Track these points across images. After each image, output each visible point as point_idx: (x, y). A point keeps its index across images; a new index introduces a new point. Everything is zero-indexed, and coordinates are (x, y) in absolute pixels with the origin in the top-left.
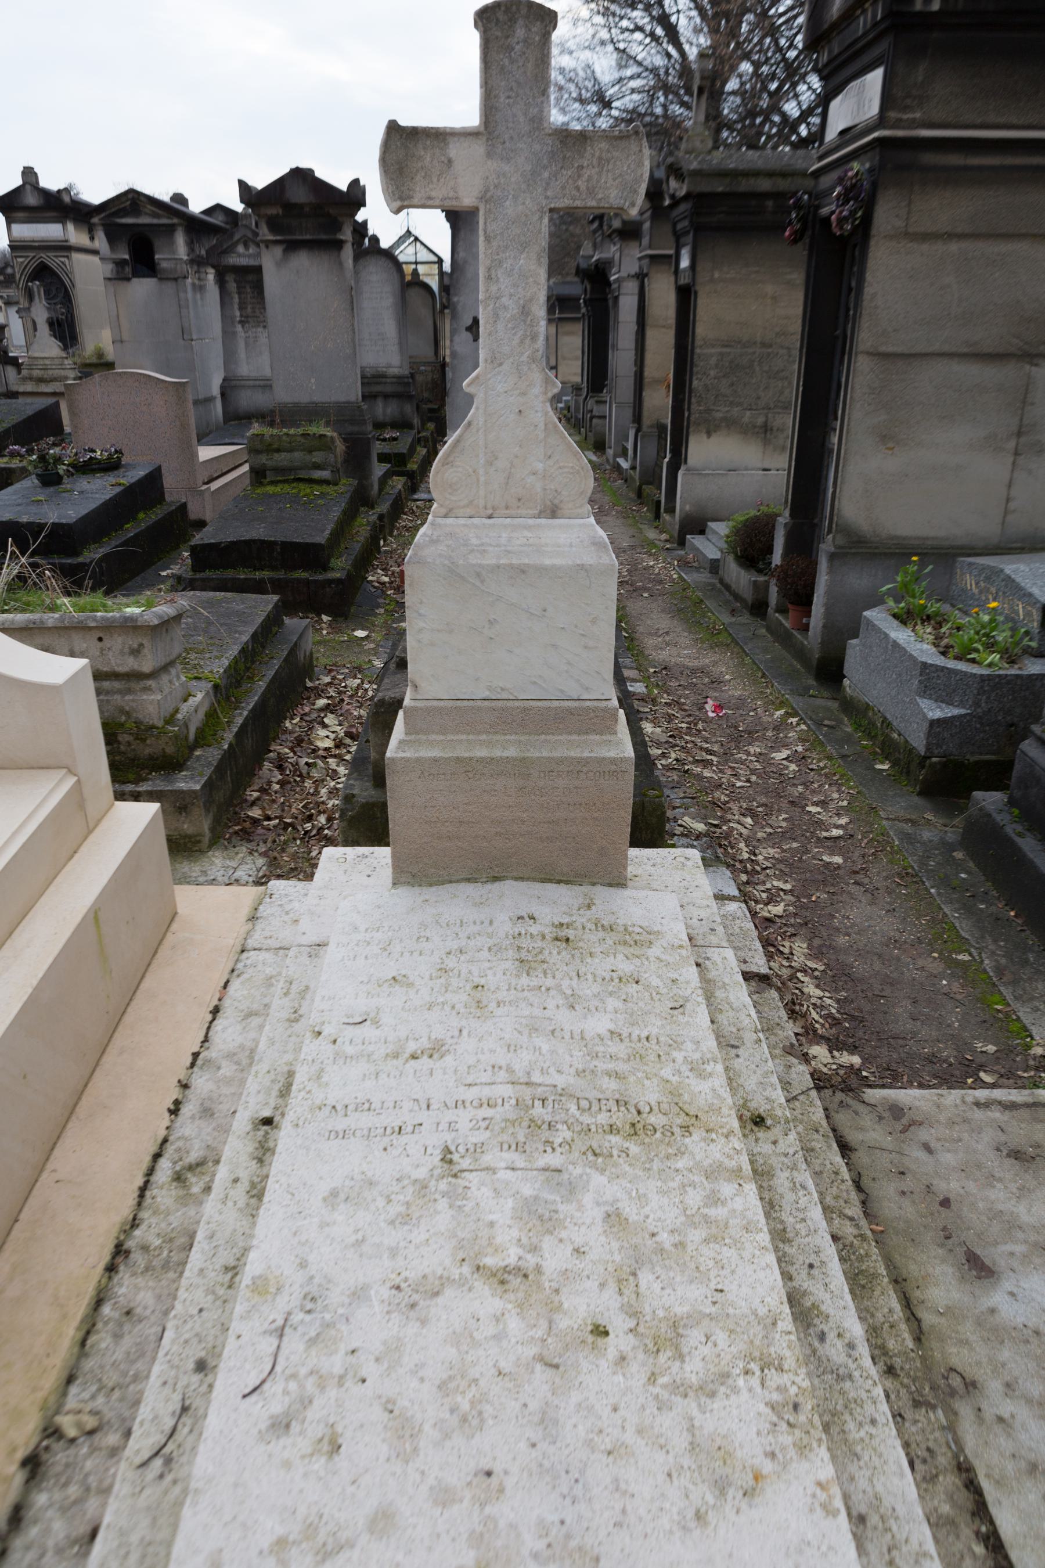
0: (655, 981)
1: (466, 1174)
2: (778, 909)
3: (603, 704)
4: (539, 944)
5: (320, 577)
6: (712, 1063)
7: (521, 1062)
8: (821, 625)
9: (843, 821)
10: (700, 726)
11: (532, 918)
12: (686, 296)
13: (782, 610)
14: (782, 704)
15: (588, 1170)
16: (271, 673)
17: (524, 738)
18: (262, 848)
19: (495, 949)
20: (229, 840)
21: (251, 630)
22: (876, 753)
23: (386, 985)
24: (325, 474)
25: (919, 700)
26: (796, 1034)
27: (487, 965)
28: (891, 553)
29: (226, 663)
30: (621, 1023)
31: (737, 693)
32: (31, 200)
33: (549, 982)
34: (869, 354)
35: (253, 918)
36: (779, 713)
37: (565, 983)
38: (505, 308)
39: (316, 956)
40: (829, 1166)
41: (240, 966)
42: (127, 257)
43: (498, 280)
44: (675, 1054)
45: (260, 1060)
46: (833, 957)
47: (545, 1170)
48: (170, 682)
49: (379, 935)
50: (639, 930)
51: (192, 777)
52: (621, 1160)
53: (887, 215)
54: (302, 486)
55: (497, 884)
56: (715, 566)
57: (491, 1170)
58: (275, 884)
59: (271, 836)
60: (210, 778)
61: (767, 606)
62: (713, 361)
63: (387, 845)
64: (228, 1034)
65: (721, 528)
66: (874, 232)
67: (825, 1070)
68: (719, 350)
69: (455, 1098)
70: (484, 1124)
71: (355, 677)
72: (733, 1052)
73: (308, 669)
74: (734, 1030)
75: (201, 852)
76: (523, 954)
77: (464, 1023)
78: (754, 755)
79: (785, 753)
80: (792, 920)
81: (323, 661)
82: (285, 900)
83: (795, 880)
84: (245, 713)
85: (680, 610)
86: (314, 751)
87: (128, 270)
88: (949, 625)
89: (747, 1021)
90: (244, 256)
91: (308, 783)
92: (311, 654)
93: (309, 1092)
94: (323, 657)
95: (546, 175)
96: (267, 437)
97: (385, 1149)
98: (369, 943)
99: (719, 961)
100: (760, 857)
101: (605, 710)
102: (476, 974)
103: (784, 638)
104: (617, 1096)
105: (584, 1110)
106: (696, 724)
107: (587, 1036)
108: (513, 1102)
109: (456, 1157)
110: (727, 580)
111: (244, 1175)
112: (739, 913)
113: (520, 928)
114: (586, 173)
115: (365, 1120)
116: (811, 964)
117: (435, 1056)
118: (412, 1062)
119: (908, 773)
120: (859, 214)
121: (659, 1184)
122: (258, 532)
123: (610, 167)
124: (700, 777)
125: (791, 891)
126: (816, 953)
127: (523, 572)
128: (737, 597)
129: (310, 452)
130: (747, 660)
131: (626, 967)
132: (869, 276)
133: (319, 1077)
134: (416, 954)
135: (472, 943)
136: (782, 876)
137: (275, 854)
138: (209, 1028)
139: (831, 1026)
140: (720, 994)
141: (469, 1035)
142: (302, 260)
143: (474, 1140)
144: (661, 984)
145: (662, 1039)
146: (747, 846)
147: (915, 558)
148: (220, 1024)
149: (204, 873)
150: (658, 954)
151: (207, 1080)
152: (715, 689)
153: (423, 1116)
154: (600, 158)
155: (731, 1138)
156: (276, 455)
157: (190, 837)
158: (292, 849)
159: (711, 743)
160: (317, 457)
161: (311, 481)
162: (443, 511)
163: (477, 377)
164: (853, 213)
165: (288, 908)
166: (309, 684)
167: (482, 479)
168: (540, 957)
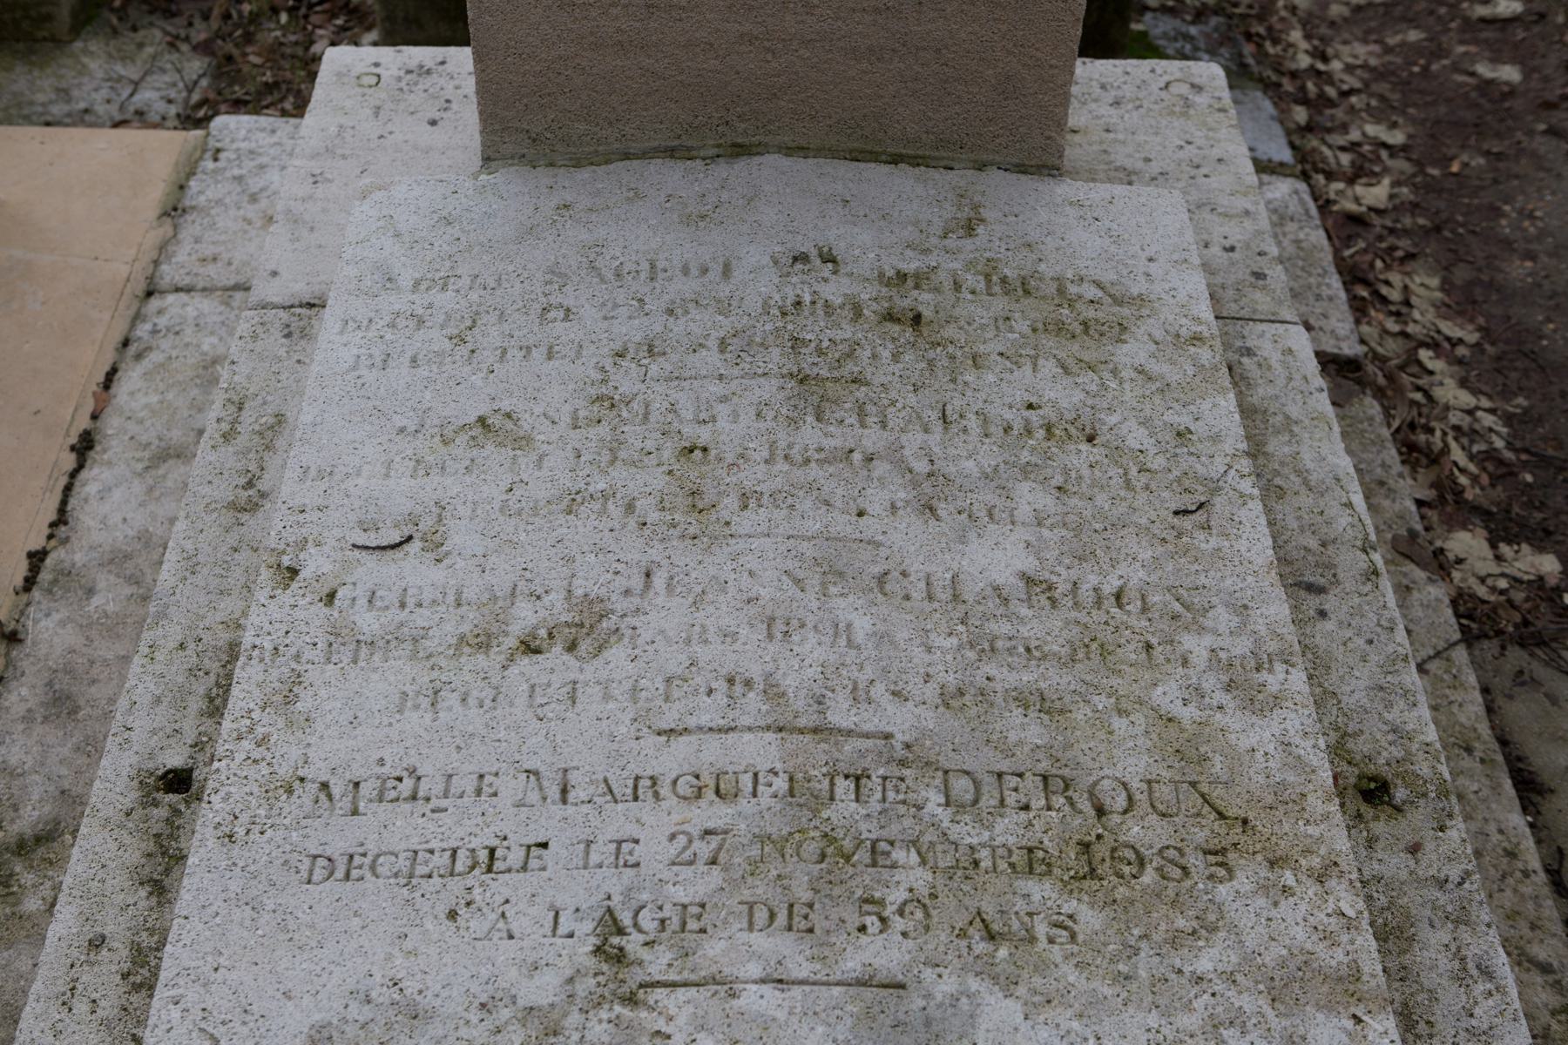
0: (1136, 437)
1: (660, 993)
2: (1376, 194)
4: (847, 332)
6: (1279, 667)
7: (801, 665)
11: (829, 259)
15: (974, 984)
18: (200, 33)
23: (462, 439)
26: (1420, 503)
27: (717, 388)
30: (1051, 555)
33: (873, 438)
35: (174, 211)
37: (913, 440)
39: (304, 334)
40: (1495, 837)
41: (143, 330)
44: (1189, 642)
45: (162, 615)
47: (861, 983)
49: (445, 300)
52: (1056, 953)
55: (741, 165)
57: (723, 984)
58: (226, 124)
63: (460, 38)
64: (112, 503)
67: (1482, 591)
69: (634, 769)
70: (704, 849)
72: (1313, 602)
74: (1313, 543)
75: (56, 41)
76: (808, 357)
77: (655, 553)
83: (1413, 121)
89: (1344, 520)
93: (262, 742)
97: (453, 915)
98: (421, 322)
99: (1275, 359)
100: (1336, 65)
104: (1044, 766)
105: (962, 807)
107: (969, 592)
108: (781, 784)
109: (632, 944)
111: (116, 927)
112: (1294, 207)
113: (798, 286)
115: (401, 829)
116: (1450, 329)
117: (584, 647)
118: (525, 662)
121: (1153, 1020)
125: (1404, 148)
126: (1460, 302)
133: (290, 699)
135: (678, 327)
137: (229, 48)
138: (68, 489)
139: (1495, 480)
140: (1277, 446)
141: (670, 587)
143: (681, 894)
144: (1148, 444)
145: (1155, 599)
148: (94, 479)
149: (64, 93)
150: (1142, 358)
151: (62, 624)
153: (548, 821)
155: (1332, 883)
158: (271, 33)
165: (255, 184)
168: (850, 368)
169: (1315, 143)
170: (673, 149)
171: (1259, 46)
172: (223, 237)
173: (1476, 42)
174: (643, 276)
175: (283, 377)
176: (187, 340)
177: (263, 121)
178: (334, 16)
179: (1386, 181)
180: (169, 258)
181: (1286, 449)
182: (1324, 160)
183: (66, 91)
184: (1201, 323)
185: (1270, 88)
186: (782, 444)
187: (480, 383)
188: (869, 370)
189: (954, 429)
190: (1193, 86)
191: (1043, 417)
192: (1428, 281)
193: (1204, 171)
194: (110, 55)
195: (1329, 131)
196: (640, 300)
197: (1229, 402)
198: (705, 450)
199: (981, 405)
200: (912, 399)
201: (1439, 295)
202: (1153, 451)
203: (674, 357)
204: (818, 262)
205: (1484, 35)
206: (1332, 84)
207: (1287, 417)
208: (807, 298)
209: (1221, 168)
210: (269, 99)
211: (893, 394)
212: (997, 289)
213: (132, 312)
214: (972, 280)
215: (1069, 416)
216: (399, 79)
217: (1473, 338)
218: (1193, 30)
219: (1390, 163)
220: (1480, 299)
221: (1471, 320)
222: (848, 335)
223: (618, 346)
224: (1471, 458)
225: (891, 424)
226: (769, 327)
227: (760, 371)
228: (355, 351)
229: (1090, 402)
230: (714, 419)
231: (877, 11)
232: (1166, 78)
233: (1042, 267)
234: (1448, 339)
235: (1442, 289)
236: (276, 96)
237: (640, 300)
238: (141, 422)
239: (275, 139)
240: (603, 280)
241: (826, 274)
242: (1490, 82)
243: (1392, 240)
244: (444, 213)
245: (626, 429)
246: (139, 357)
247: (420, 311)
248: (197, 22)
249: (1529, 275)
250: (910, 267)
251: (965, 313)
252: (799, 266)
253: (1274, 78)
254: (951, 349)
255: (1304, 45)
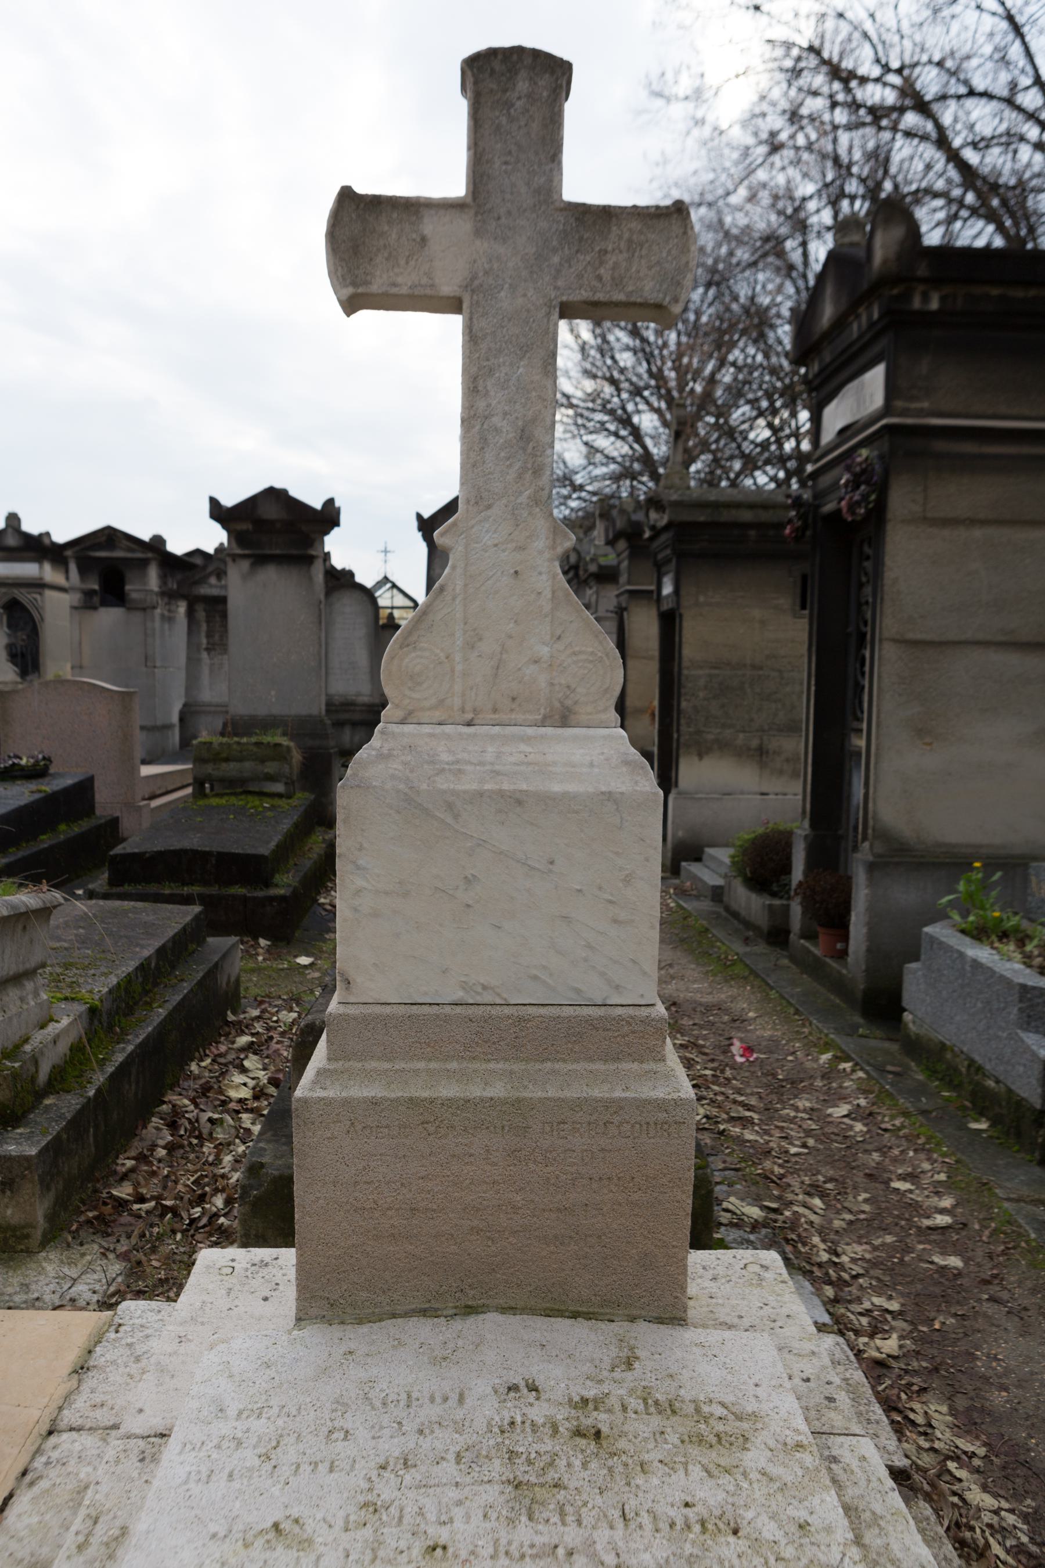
0: (770, 1530)
2: (890, 1345)
3: (644, 1012)
4: (548, 1445)
5: (260, 894)
8: (864, 948)
9: (947, 1202)
10: (728, 1073)
11: (533, 1388)
12: (670, 623)
13: (809, 935)
14: (827, 1046)
16: (178, 998)
17: (516, 1067)
18: (123, 1247)
19: (468, 1456)
20: (75, 1234)
21: (158, 944)
22: (965, 1108)
23: (260, 1542)
24: (279, 788)
25: (1023, 1035)
27: (453, 1494)
28: (948, 863)
29: (113, 980)
31: (767, 1034)
32: (11, 541)
33: (572, 1535)
34: (895, 641)
35: (81, 1369)
36: (825, 1057)
37: (602, 1536)
38: (497, 430)
41: (39, 1462)
42: (96, 587)
43: (487, 394)
46: (993, 1430)
48: (22, 999)
49: (259, 1425)
50: (719, 1411)
51: (29, 1137)
53: (902, 500)
54: (250, 798)
55: (471, 1320)
56: (717, 894)
59: (139, 1226)
60: (57, 1138)
61: (788, 932)
62: (702, 682)
63: (290, 1244)
65: (723, 855)
66: (890, 515)
68: (707, 671)
71: (291, 1010)
73: (232, 999)
75: (29, 1252)
78: (805, 1111)
79: (843, 1109)
80: (915, 1364)
81: (254, 991)
82: (139, 1335)
83: (902, 1294)
84: (130, 1048)
85: (682, 940)
86: (224, 1103)
87: (96, 600)
88: (1035, 942)
90: (216, 587)
91: (208, 1148)
92: (238, 981)
94: (252, 986)
95: (556, 259)
96: (216, 746)
99: (855, 1464)
100: (845, 1259)
101: (647, 1021)
102: (432, 1517)
103: (814, 968)
106: (723, 1071)
110: (734, 906)
114: (611, 259)
116: (965, 1445)
119: (1019, 1135)
120: (873, 497)
122: (193, 841)
123: (644, 252)
124: (740, 1141)
125: (901, 1313)
126: (968, 1422)
127: (519, 802)
128: (748, 924)
129: (263, 761)
130: (773, 994)
131: (711, 1495)
132: (888, 561)
134: (323, 1468)
135: (426, 1443)
136: (881, 1288)
137: (141, 1256)
142: (270, 574)
144: (779, 1535)
146: (824, 1241)
147: (977, 864)
149: (25, 1287)
150: (762, 1463)
152: (738, 1029)
154: (630, 241)
156: (224, 765)
157: (14, 1229)
158: (169, 1246)
159: (746, 1095)
160: (270, 768)
161: (262, 794)
162: (399, 714)
163: (455, 524)
164: (865, 497)
165: (140, 1349)
166: (231, 1017)
167: (459, 668)
168: (552, 1475)
169: (843, 1311)
170: (425, 1310)
171: (795, 1247)
172: (112, 1388)
173: (929, 1242)
174: (402, 1404)
175: (132, 1495)
176: (70, 1469)
177: (154, 1304)
178: (211, 1235)
179: (895, 1336)
180: (70, 1404)
181: (879, 1541)
182: (851, 1322)
183: (27, 1286)
184: (800, 1434)
185: (807, 1274)
186: (503, 1541)
187: (277, 1493)
188: (566, 1476)
189: (633, 1525)
190: (762, 1266)
191: (697, 1514)
192: (939, 1408)
193: (779, 1324)
194: (62, 1262)
195: (850, 1302)
196: (400, 1423)
197: (831, 1498)
198: (444, 1548)
199: (650, 1504)
200: (599, 1500)
201: (949, 1418)
202: (783, 1542)
203: (423, 1468)
204: (525, 1391)
205: (933, 1237)
206: (845, 1271)
207: (874, 1513)
208: (519, 1419)
209: (790, 1321)
210: (160, 1290)
211: (585, 1497)
212: (652, 1410)
213: (34, 1448)
214: (634, 1403)
215: (717, 1512)
216: (247, 1270)
217: (982, 1451)
218: (752, 1237)
219: (893, 1323)
220: (978, 1421)
221: (977, 1438)
222: (549, 1448)
223: (381, 1460)
224: (1008, 1552)
225: (585, 1522)
226: (492, 1442)
227: (486, 1479)
228: (188, 1469)
229: (730, 1500)
230: (451, 1520)
231: (559, 1210)
232: (744, 1261)
233: (682, 1392)
234: (965, 1453)
235: (952, 1415)
236: (166, 1288)
237: (400, 1423)
238: (21, 1540)
239: (160, 1317)
240: (373, 1408)
241: (532, 1400)
242: (944, 1268)
243: (907, 1379)
244: (266, 1359)
245: (385, 1531)
246: (32, 1484)
247: (239, 1435)
248: (123, 1240)
249: (1007, 1402)
250: (590, 1394)
251: (631, 1429)
252: (512, 1394)
253: (808, 1267)
254: (624, 1458)
255: (822, 1246)
